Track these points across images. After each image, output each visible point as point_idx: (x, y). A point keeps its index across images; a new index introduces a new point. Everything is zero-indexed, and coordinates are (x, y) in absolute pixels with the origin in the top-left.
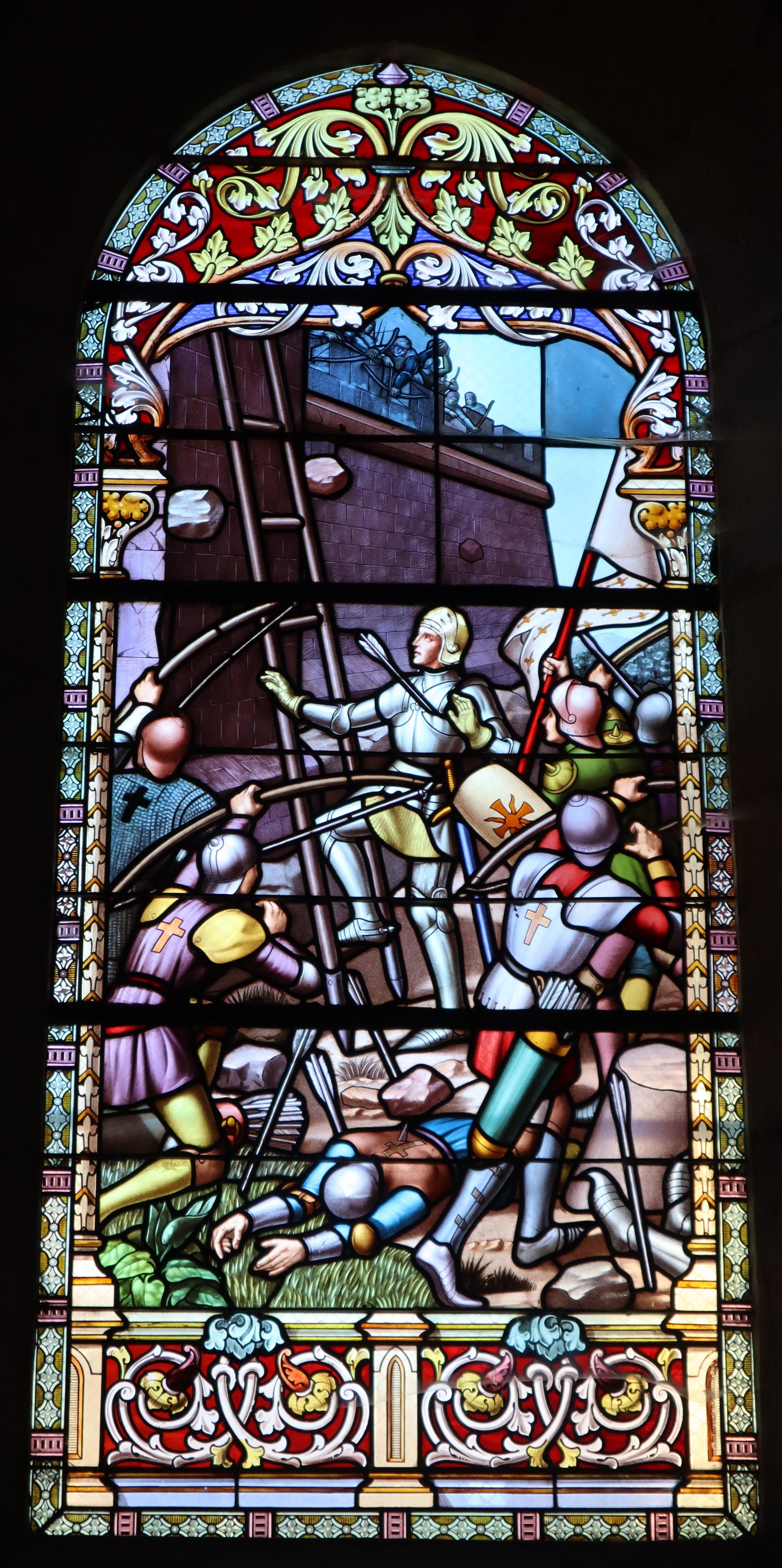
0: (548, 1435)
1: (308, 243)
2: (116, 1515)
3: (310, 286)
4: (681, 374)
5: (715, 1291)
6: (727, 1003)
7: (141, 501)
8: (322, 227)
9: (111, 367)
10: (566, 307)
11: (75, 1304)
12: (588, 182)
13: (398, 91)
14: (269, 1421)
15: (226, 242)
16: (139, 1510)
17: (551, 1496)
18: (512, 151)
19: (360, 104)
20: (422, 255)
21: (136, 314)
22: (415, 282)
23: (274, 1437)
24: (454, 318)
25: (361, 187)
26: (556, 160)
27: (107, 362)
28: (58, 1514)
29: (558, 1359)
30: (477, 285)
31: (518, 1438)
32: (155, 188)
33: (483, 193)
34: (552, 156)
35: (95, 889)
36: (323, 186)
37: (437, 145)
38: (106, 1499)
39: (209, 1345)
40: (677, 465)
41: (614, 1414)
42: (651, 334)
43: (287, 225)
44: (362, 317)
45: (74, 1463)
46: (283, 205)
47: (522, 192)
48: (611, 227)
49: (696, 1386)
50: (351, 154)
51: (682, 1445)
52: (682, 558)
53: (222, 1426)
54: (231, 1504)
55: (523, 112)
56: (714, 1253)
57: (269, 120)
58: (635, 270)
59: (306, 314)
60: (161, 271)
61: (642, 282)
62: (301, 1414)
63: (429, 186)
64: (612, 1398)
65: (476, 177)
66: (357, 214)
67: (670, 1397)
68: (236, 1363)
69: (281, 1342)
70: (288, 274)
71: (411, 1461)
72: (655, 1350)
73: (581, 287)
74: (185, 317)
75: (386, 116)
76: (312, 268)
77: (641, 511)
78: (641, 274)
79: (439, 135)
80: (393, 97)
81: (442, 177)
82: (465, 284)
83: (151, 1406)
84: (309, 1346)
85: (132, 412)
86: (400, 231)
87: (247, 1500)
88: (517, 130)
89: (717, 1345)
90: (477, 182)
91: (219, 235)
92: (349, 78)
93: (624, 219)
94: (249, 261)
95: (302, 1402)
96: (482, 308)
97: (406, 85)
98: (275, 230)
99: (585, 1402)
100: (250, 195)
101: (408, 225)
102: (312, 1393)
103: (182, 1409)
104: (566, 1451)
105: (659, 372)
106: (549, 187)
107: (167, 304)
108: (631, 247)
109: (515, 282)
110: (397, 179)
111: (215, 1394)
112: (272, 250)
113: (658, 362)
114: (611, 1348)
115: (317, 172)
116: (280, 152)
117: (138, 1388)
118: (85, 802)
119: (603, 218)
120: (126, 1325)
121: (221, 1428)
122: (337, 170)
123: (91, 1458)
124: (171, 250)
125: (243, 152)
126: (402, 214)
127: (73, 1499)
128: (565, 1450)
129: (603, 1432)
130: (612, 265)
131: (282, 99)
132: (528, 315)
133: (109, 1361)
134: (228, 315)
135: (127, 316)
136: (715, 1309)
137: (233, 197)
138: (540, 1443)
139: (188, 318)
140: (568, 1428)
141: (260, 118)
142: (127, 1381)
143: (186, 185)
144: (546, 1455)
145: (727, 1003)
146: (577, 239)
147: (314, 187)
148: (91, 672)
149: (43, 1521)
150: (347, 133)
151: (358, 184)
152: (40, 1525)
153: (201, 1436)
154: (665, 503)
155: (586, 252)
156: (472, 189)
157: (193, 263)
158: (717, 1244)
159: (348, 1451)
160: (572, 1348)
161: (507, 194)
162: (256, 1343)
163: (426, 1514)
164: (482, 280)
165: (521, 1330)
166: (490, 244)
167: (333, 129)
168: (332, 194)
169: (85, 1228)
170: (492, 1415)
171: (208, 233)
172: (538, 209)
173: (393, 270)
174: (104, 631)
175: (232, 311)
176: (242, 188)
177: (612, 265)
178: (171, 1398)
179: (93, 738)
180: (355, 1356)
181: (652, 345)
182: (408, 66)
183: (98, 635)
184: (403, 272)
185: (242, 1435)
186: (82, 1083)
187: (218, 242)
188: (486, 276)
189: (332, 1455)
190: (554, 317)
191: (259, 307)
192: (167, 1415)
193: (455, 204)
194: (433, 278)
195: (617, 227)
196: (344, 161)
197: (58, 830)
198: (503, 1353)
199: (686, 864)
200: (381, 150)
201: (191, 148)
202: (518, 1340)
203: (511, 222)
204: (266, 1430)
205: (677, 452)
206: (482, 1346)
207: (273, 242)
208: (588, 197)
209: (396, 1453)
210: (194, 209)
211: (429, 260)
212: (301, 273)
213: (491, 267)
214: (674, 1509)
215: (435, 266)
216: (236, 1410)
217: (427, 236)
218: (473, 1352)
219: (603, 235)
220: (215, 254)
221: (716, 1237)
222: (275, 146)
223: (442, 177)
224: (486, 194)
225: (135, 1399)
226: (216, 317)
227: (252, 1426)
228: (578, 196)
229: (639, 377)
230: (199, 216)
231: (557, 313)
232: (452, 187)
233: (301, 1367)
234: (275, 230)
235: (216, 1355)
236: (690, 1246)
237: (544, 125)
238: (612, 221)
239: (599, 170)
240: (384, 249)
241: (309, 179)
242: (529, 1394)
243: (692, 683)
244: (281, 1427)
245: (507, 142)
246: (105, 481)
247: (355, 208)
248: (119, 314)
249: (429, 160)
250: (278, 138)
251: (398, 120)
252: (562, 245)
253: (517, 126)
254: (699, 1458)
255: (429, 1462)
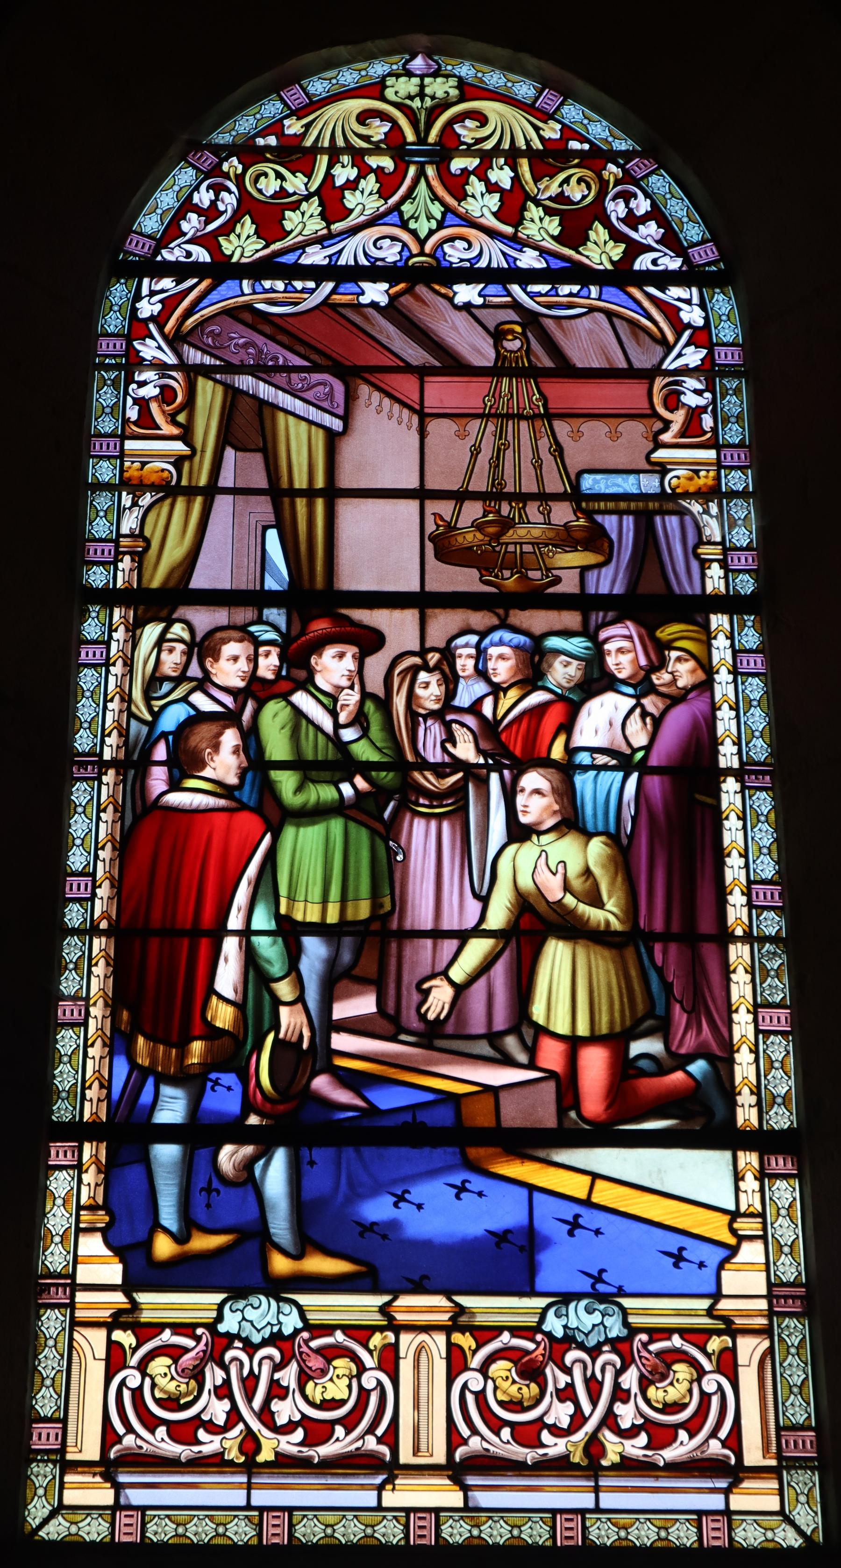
0: (589, 1427)
1: (337, 227)
2: (118, 1513)
3: (341, 266)
4: (710, 347)
5: (764, 1274)
6: (746, 585)
7: (163, 470)
8: (351, 211)
9: (135, 343)
10: (593, 284)
11: (79, 1281)
12: (618, 167)
13: (427, 80)
14: (284, 1411)
15: (254, 226)
16: (143, 1509)
17: (593, 1495)
18: (541, 138)
19: (389, 93)
20: (451, 239)
21: (163, 291)
22: (445, 264)
23: (289, 1428)
24: (480, 295)
25: (390, 174)
26: (586, 147)
27: (129, 339)
28: (53, 1515)
29: (599, 1345)
30: (506, 266)
31: (556, 1431)
32: (185, 176)
33: (512, 178)
34: (582, 143)
35: (104, 925)
36: (353, 173)
37: (467, 132)
38: (105, 1496)
39: (222, 1328)
40: (709, 435)
41: (660, 1406)
42: (680, 309)
43: (316, 209)
44: (389, 295)
45: (69, 1457)
46: (312, 190)
47: (552, 176)
48: (641, 212)
49: (748, 1378)
50: (381, 141)
51: (734, 1441)
52: (714, 524)
53: (234, 1416)
54: (243, 1502)
55: (549, 105)
56: (761, 1233)
57: (297, 110)
58: (666, 254)
59: (334, 291)
60: (189, 254)
61: (674, 264)
62: (318, 1402)
63: (459, 172)
64: (657, 1388)
65: (505, 164)
66: (386, 200)
67: (720, 1388)
68: (250, 1348)
69: (300, 1325)
70: (315, 256)
71: (440, 1457)
72: (702, 1337)
73: (609, 267)
74: (209, 297)
75: (416, 104)
76: (340, 252)
77: (671, 479)
78: (671, 257)
79: (469, 123)
80: (422, 86)
81: (473, 163)
82: (494, 265)
83: (158, 1395)
84: (327, 1329)
85: (155, 387)
86: (429, 217)
87: (260, 1498)
88: (547, 117)
89: (766, 1332)
90: (506, 168)
91: (247, 219)
92: (378, 69)
93: (654, 204)
94: (278, 244)
95: (319, 1389)
96: (508, 286)
97: (435, 75)
98: (303, 214)
99: (628, 1391)
100: (279, 181)
101: (437, 210)
102: (331, 1380)
103: (191, 1398)
104: (608, 1446)
105: (687, 344)
106: (578, 172)
107: (195, 280)
108: (662, 231)
109: (545, 265)
110: (427, 166)
111: (227, 1382)
112: (300, 234)
113: (687, 334)
114: (657, 1333)
115: (345, 159)
116: (309, 142)
117: (144, 1374)
118: (93, 875)
119: (633, 204)
120: (135, 1306)
121: (234, 1417)
122: (366, 158)
123: (92, 1452)
124: (199, 234)
125: (272, 141)
126: (432, 200)
127: (71, 1497)
128: (607, 1445)
129: (648, 1425)
130: (640, 249)
131: (311, 89)
132: (557, 291)
133: (113, 1346)
134: (254, 293)
135: (152, 293)
136: (764, 1292)
137: (262, 183)
138: (580, 1436)
139: (214, 296)
140: (610, 1420)
141: (289, 108)
142: (133, 1367)
143: (216, 171)
144: (587, 1450)
145: (746, 585)
146: (607, 224)
147: (344, 173)
148: (103, 736)
149: (38, 1521)
150: (377, 122)
151: (387, 171)
152: (34, 1526)
153: (212, 1428)
154: (696, 472)
155: (616, 236)
156: (502, 176)
157: (220, 246)
158: (764, 1223)
159: (371, 1443)
160: (613, 1334)
161: (536, 179)
162: (272, 1325)
163: (456, 1515)
164: (511, 260)
165: (558, 1315)
166: (520, 229)
167: (363, 117)
168: (362, 180)
169: (116, 758)
170: (525, 1404)
171: (236, 218)
172: (567, 192)
173: (422, 253)
174: (120, 659)
175: (258, 289)
176: (272, 174)
177: (640, 249)
178: (179, 1386)
179: (96, 923)
180: (714, 1344)
181: (681, 320)
182: (436, 58)
183: (112, 700)
184: (432, 255)
185: (256, 1425)
186: (116, 630)
187: (247, 227)
188: (516, 259)
189: (353, 1447)
190: (582, 293)
191: (286, 285)
192: (174, 1405)
193: (484, 191)
194: (462, 260)
195: (647, 212)
196: (376, 150)
197: (56, 1030)
198: (539, 1337)
199: (720, 748)
200: (410, 137)
201: (223, 138)
202: (554, 1325)
203: (540, 209)
204: (281, 1420)
205: (707, 421)
206: (516, 1331)
207: (300, 226)
208: (617, 182)
209: (423, 1447)
210: (224, 194)
211: (460, 244)
212: (330, 256)
213: (521, 251)
214: (727, 1512)
215: (464, 249)
216: (249, 1397)
217: (457, 221)
218: (506, 1337)
219: (633, 221)
220: (243, 237)
221: (762, 1215)
222: (303, 135)
223: (473, 163)
224: (516, 180)
225: (141, 1387)
226: (243, 294)
227: (266, 1416)
228: (608, 181)
229: (669, 348)
230: (229, 201)
231: (585, 289)
232: (481, 173)
233: (319, 1351)
234: (303, 214)
235: (230, 1339)
236: (736, 1226)
237: (572, 112)
238: (642, 206)
239: (628, 155)
240: (414, 233)
241: (338, 166)
242: (567, 1383)
243: (743, 860)
244: (297, 1417)
245: (537, 129)
246: (127, 452)
247: (384, 193)
248: (145, 291)
249: (457, 149)
250: (308, 126)
251: (426, 109)
252: (591, 229)
253: (547, 114)
254: (753, 1455)
255: (457, 1457)
